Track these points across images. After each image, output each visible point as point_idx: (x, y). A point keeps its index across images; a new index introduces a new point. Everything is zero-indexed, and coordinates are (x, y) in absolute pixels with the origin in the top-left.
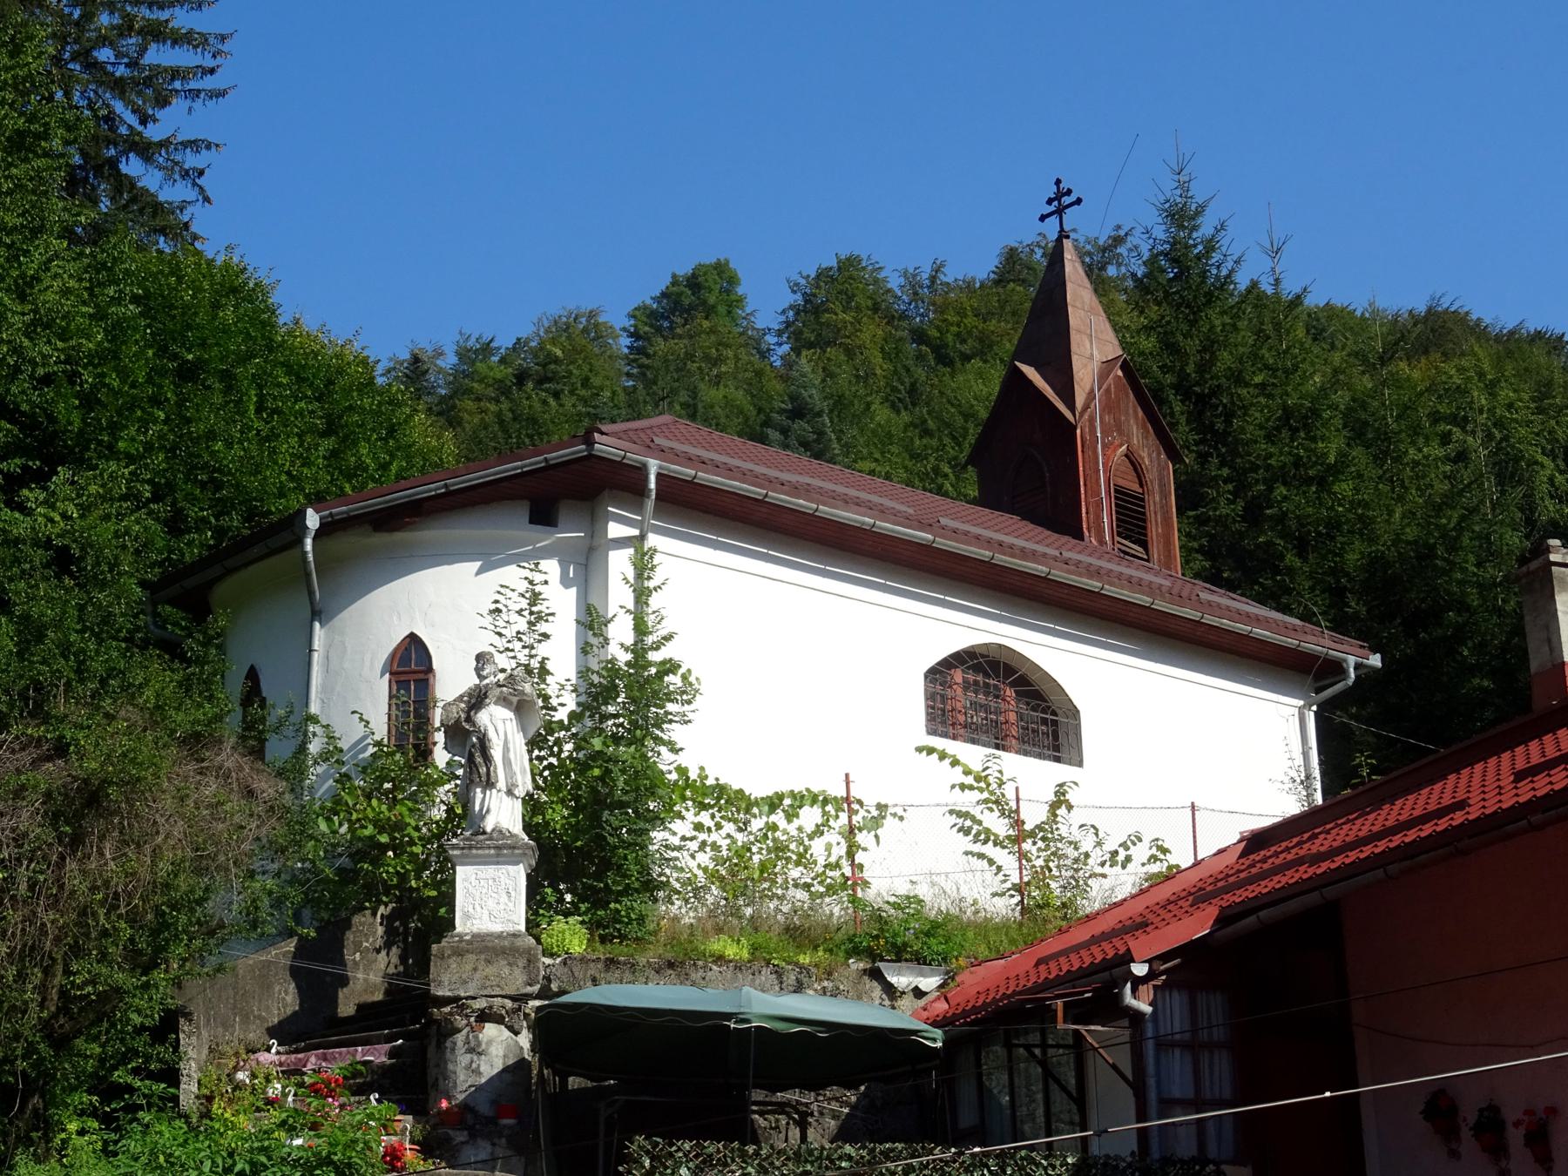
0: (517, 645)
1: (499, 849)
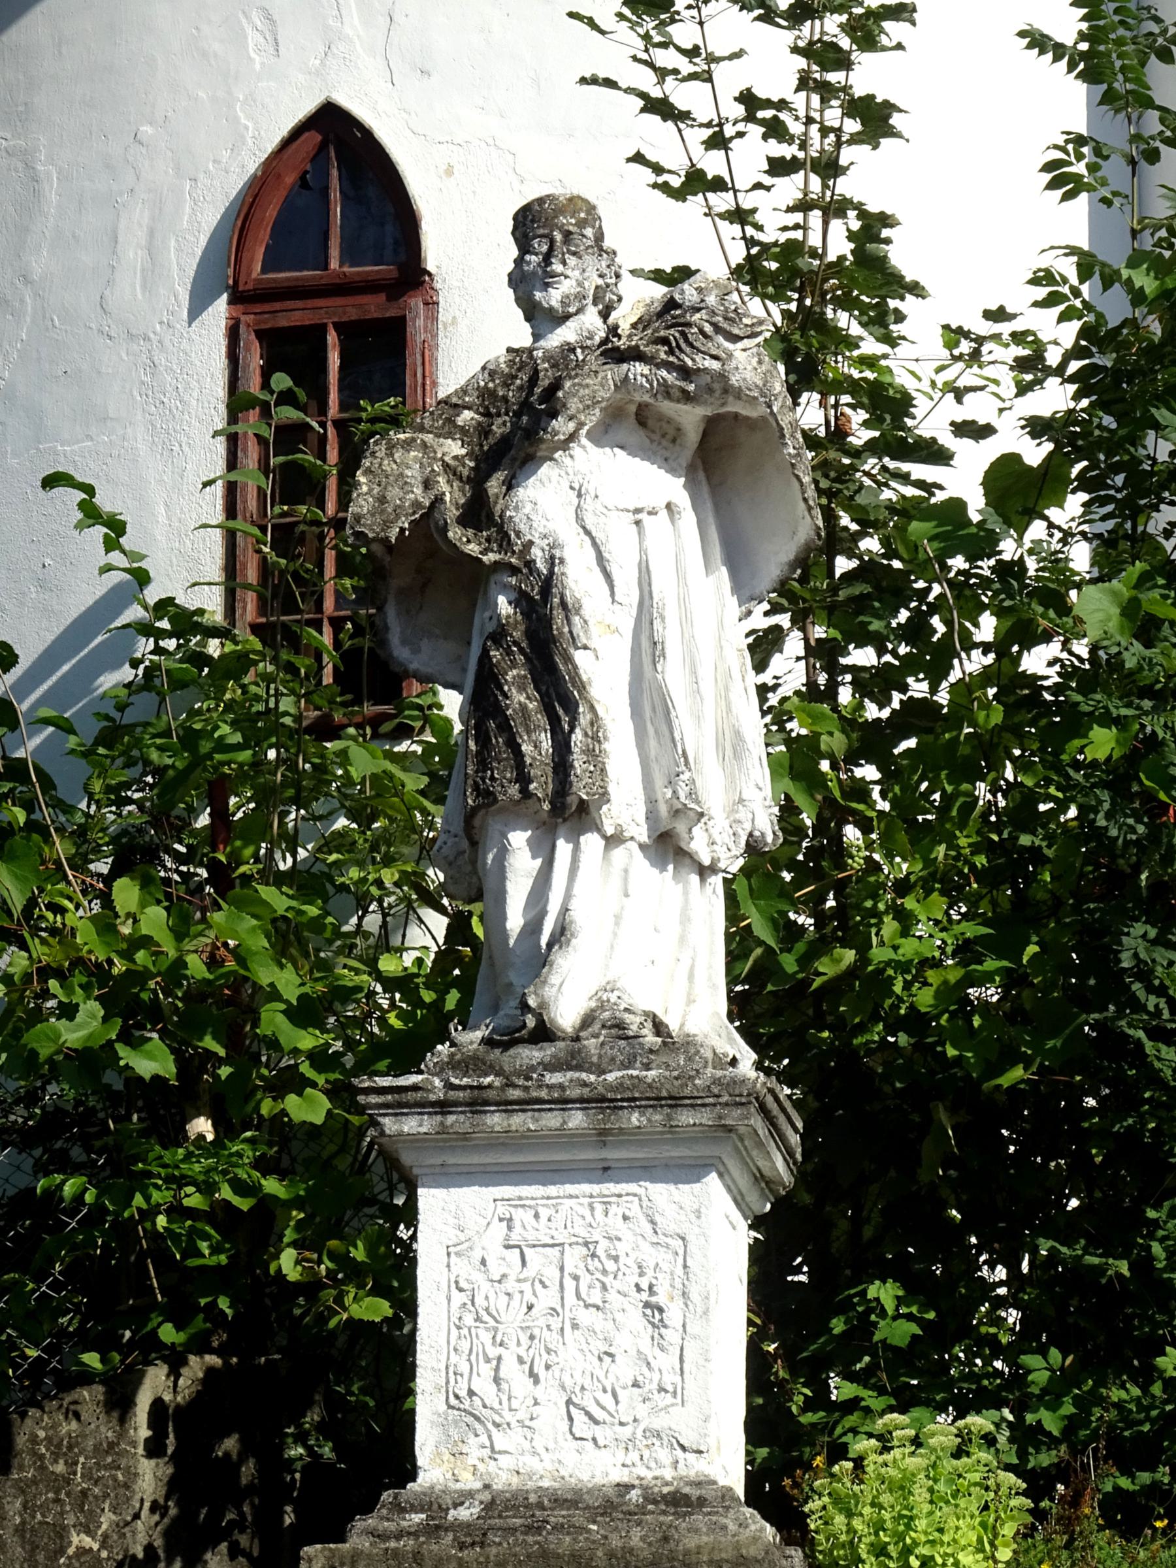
0: (752, 152)
1: (618, 1108)
